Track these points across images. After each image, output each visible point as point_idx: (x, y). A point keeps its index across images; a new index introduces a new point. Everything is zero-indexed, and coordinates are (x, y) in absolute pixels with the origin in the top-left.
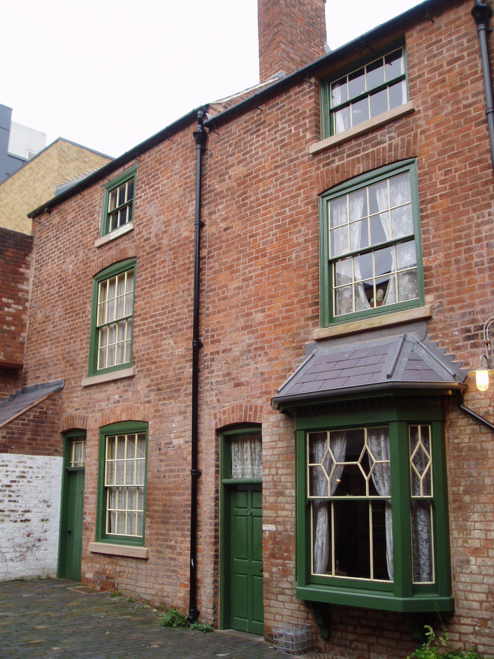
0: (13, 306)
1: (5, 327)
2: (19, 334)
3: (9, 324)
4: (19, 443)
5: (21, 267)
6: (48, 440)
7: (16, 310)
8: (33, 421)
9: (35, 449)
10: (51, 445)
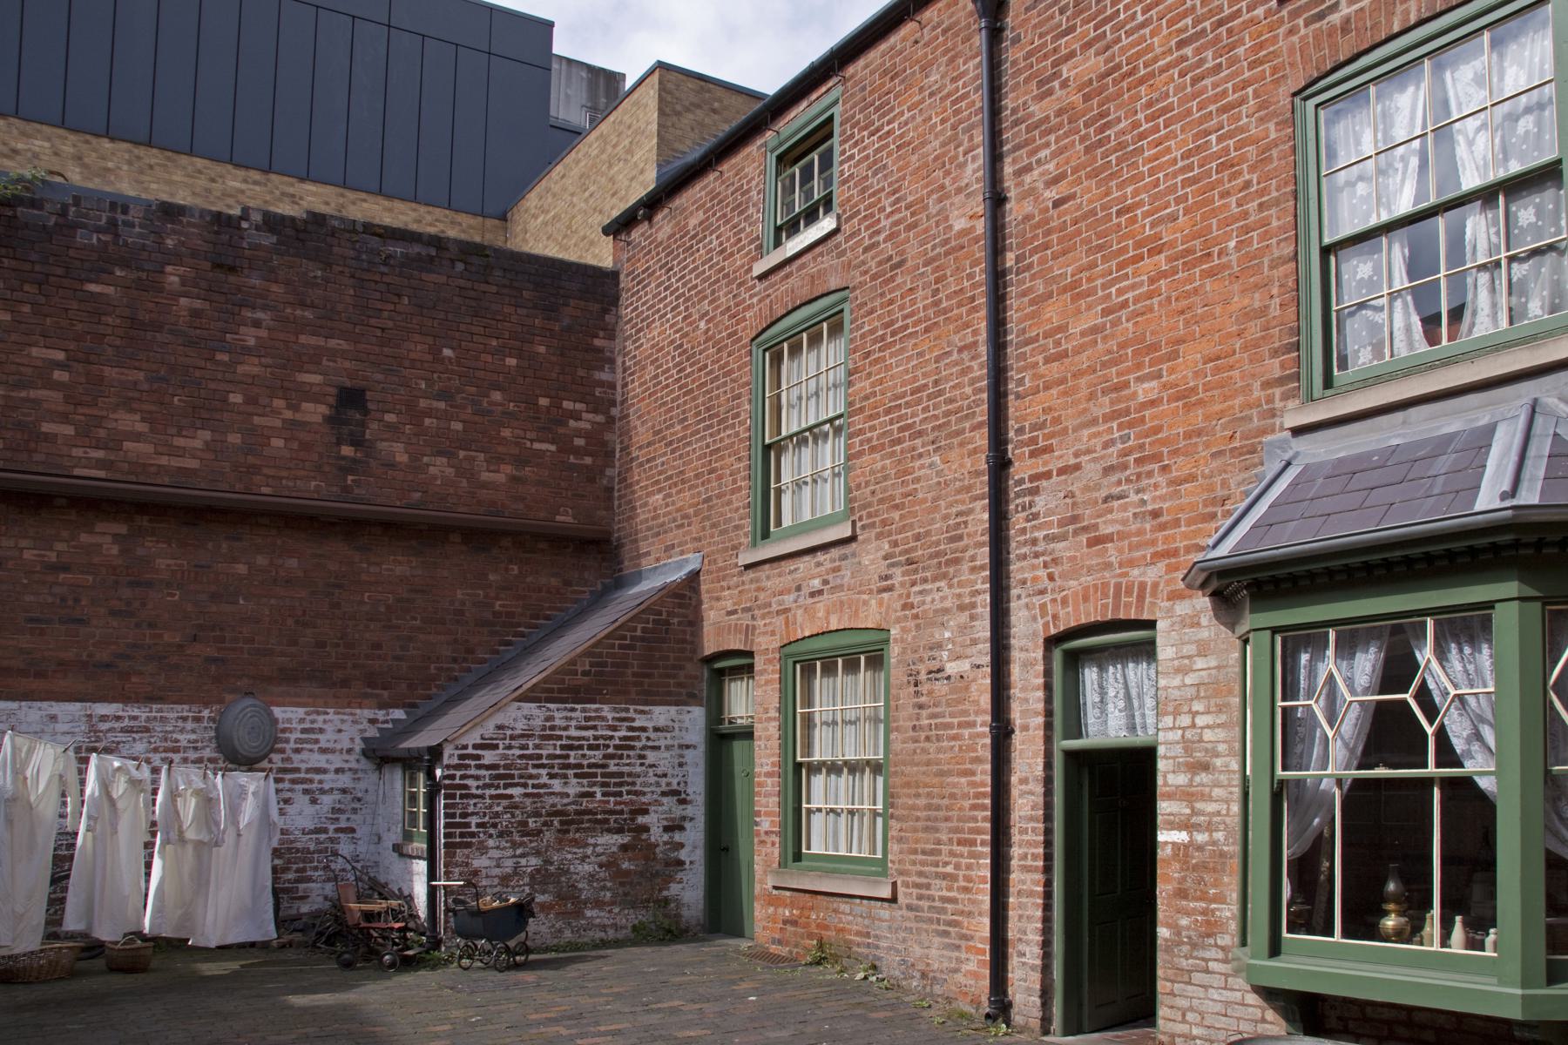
1: (572, 459)
2: (602, 472)
3: (577, 452)
6: (674, 676)
7: (593, 423)
8: (642, 639)
10: (680, 685)
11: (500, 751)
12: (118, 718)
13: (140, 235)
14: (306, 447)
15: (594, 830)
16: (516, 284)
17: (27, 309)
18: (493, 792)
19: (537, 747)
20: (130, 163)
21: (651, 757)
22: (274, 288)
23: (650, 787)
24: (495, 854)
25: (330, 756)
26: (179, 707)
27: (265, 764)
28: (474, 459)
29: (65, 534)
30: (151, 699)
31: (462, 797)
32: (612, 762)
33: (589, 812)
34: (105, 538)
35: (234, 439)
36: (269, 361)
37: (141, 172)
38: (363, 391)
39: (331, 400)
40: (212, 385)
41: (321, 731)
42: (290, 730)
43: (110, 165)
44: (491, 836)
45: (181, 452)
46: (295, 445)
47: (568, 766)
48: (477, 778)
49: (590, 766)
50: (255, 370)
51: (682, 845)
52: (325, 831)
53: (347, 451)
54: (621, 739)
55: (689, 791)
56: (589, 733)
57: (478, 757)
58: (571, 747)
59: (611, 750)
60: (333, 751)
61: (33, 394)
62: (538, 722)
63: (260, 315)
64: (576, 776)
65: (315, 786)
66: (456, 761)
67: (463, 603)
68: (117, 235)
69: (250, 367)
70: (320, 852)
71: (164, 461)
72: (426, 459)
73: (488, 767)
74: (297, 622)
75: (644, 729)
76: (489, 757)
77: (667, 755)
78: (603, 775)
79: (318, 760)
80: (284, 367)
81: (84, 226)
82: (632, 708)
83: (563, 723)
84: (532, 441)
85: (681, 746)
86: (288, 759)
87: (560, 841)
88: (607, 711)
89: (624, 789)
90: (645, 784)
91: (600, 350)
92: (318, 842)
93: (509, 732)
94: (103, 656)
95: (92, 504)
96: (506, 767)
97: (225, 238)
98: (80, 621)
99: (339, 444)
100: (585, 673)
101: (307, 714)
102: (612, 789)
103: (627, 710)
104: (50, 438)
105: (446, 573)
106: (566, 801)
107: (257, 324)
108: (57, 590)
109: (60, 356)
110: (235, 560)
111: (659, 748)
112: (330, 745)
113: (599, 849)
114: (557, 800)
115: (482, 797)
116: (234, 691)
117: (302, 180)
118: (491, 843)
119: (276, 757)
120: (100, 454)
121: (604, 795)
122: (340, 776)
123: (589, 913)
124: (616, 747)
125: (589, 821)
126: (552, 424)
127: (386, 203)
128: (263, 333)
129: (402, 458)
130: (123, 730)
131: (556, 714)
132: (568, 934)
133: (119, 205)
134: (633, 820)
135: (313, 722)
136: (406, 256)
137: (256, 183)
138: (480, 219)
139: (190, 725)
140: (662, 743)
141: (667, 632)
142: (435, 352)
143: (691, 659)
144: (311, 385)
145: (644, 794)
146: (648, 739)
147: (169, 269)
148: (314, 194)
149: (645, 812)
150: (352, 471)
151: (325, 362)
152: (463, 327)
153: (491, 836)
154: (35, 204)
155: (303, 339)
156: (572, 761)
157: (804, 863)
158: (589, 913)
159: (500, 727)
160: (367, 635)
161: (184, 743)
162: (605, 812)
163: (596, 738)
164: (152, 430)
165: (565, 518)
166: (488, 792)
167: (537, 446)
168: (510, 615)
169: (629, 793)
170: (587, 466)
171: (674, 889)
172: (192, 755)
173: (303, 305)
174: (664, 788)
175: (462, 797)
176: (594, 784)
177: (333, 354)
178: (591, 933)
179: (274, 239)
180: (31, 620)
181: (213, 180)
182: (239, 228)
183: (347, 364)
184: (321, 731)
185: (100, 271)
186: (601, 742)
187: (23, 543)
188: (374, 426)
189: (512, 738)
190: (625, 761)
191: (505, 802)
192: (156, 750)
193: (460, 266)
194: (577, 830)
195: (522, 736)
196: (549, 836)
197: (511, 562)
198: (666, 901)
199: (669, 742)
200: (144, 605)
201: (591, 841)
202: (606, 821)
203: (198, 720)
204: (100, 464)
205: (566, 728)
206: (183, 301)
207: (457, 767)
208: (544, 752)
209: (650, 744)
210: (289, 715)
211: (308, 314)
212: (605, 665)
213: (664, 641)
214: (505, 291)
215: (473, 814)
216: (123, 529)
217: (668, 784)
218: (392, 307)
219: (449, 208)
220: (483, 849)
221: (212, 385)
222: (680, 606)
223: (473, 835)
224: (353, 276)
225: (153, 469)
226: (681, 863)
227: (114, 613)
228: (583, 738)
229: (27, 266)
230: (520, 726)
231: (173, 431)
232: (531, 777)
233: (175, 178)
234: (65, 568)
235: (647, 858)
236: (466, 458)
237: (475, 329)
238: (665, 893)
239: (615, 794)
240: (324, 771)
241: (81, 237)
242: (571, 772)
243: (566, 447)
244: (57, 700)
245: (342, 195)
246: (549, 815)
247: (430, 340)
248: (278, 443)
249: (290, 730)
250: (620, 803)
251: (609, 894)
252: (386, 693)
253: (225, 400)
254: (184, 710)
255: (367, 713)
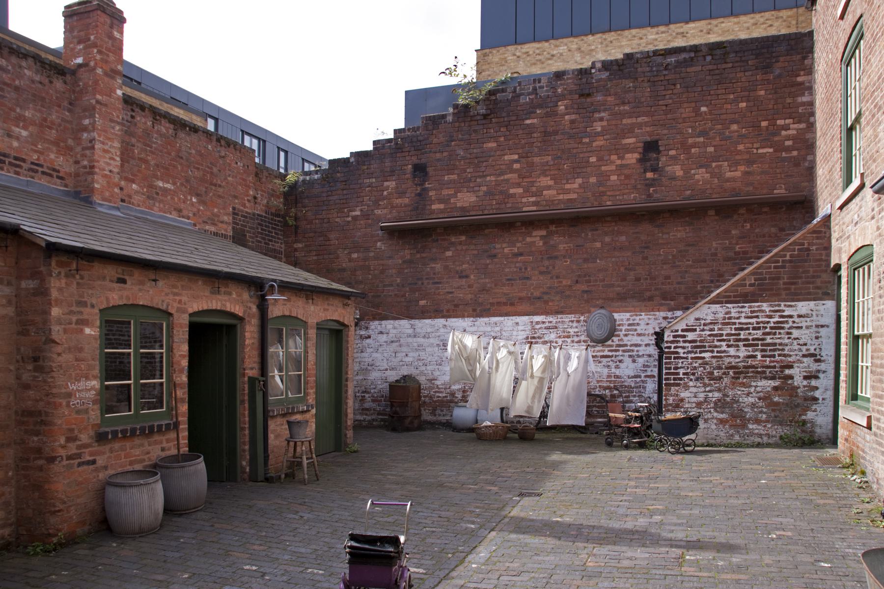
0: (791, 126)
1: (784, 154)
2: (805, 159)
3: (788, 149)
4: (772, 290)
5: (799, 75)
6: (813, 283)
7: (797, 130)
8: (790, 261)
9: (796, 294)
10: (818, 288)
11: (698, 332)
12: (544, 322)
13: (547, 91)
14: (627, 177)
15: (756, 377)
16: (743, 59)
17: (502, 139)
18: (693, 355)
19: (720, 329)
20: (601, 43)
21: (796, 333)
22: (609, 99)
23: (793, 351)
24: (694, 390)
25: (642, 338)
26: (570, 316)
27: (610, 342)
28: (721, 166)
29: (520, 239)
30: (557, 312)
31: (675, 358)
32: (768, 337)
33: (753, 367)
34: (536, 237)
35: (593, 180)
36: (608, 137)
37: (607, 46)
38: (657, 142)
39: (641, 150)
40: (581, 155)
41: (638, 324)
42: (622, 325)
43: (593, 47)
44: (691, 380)
45: (568, 191)
46: (623, 177)
47: (740, 340)
48: (684, 348)
49: (753, 340)
50: (601, 143)
51: (817, 388)
52: (640, 377)
53: (649, 175)
54: (774, 323)
55: (823, 354)
56: (754, 320)
57: (684, 336)
58: (742, 329)
59: (768, 330)
60: (644, 335)
61: (506, 177)
62: (721, 315)
63: (603, 114)
64: (744, 345)
65: (635, 353)
66: (672, 339)
67: (716, 249)
68: (537, 94)
69: (599, 142)
70: (637, 387)
71: (561, 197)
72: (693, 172)
73: (690, 342)
74: (626, 269)
75: (791, 316)
76: (691, 336)
77: (807, 331)
78: (762, 345)
79: (636, 340)
80: (616, 138)
81: (523, 94)
82: (782, 304)
83: (737, 315)
84: (757, 149)
85: (817, 326)
86: (621, 340)
87: (733, 384)
88: (765, 307)
89: (776, 353)
90: (791, 350)
91: (802, 83)
92: (636, 382)
93: (703, 322)
94: (537, 294)
95: (531, 223)
96: (701, 341)
97: (584, 80)
98: (528, 278)
99: (645, 172)
100: (751, 285)
101: (631, 316)
102: (768, 353)
103: (779, 305)
104: (513, 196)
105: (706, 233)
106: (737, 360)
107: (601, 119)
108: (517, 265)
109: (516, 157)
110: (595, 241)
111: (801, 328)
112: (643, 332)
113: (759, 389)
114: (732, 360)
115: (686, 358)
116: (595, 306)
117: (687, 23)
118: (691, 384)
119: (615, 339)
120: (533, 199)
121: (762, 356)
122: (648, 348)
123: (750, 426)
124: (771, 328)
125: (753, 372)
126: (770, 136)
127: (736, 20)
128: (605, 123)
129: (679, 173)
130: (546, 328)
131: (732, 310)
132: (737, 437)
133: (537, 79)
134: (782, 372)
135: (634, 320)
136: (677, 62)
137: (662, 33)
138: (795, 10)
139: (575, 324)
140: (804, 324)
141: (808, 255)
142: (697, 111)
143: (826, 271)
144: (630, 144)
145: (790, 356)
146: (794, 322)
147: (560, 103)
148: (694, 28)
149: (791, 367)
150: (651, 185)
151: (636, 131)
152: (712, 92)
153: (691, 380)
154: (503, 91)
155: (625, 121)
156: (742, 337)
157: (859, 402)
158: (750, 426)
159: (697, 319)
160: (662, 272)
161: (572, 333)
162: (763, 367)
163: (758, 323)
164: (555, 183)
165: (780, 191)
166: (690, 356)
167: (760, 151)
168: (745, 253)
169: (779, 355)
170: (794, 157)
171: (810, 415)
172: (576, 339)
173: (624, 103)
174: (804, 352)
175: (675, 358)
176: (757, 350)
177: (640, 125)
178: (752, 438)
179: (607, 74)
180: (508, 280)
181: (641, 38)
182: (591, 73)
183: (648, 129)
184: (638, 324)
185: (530, 113)
186: (762, 325)
187: (504, 245)
188: (664, 159)
189: (705, 325)
190: (777, 336)
191: (700, 361)
192: (560, 337)
193: (709, 58)
194: (745, 378)
195: (711, 323)
196: (726, 380)
197: (745, 221)
198: (804, 422)
199: (809, 324)
200: (554, 268)
201: (753, 384)
202: (764, 372)
203: (578, 321)
204: (535, 204)
205: (738, 318)
206: (567, 117)
207: (672, 342)
208: (724, 332)
209: (795, 325)
210: (622, 317)
211: (627, 108)
212: (765, 279)
213: (806, 261)
214: (736, 65)
215: (681, 367)
216: (544, 233)
217: (807, 350)
218: (670, 92)
219: (775, 9)
220: (687, 387)
221: (581, 155)
222: (818, 238)
223: (681, 379)
224: (649, 81)
225: (556, 202)
226: (815, 399)
227: (541, 273)
228: (750, 323)
229: (502, 120)
230: (709, 318)
231: (564, 182)
232: (716, 347)
233: (623, 43)
234: (521, 254)
235: (791, 396)
236: (716, 166)
237: (719, 92)
238: (804, 417)
239: (770, 356)
240: (640, 345)
241: (522, 100)
242: (741, 344)
243: (779, 148)
244: (519, 315)
245: (710, 24)
246: (727, 368)
247: (693, 105)
248: (614, 178)
249: (622, 325)
250: (774, 362)
251: (764, 416)
252: (672, 303)
253: (588, 162)
254: (572, 317)
255: (663, 314)
